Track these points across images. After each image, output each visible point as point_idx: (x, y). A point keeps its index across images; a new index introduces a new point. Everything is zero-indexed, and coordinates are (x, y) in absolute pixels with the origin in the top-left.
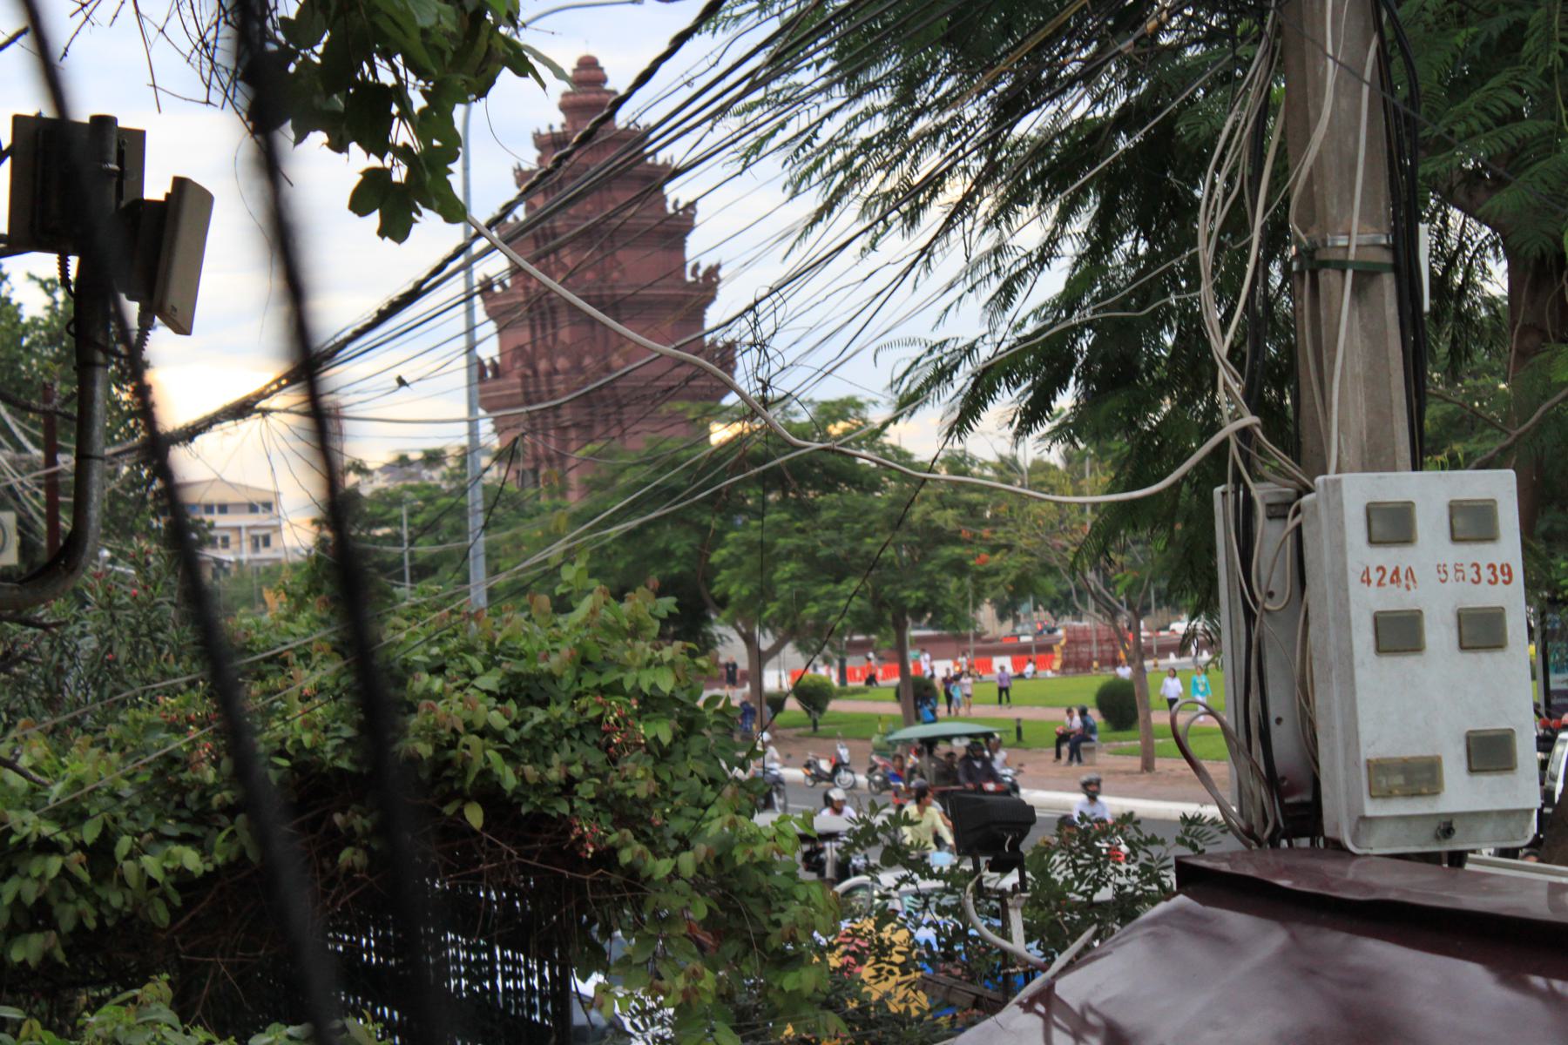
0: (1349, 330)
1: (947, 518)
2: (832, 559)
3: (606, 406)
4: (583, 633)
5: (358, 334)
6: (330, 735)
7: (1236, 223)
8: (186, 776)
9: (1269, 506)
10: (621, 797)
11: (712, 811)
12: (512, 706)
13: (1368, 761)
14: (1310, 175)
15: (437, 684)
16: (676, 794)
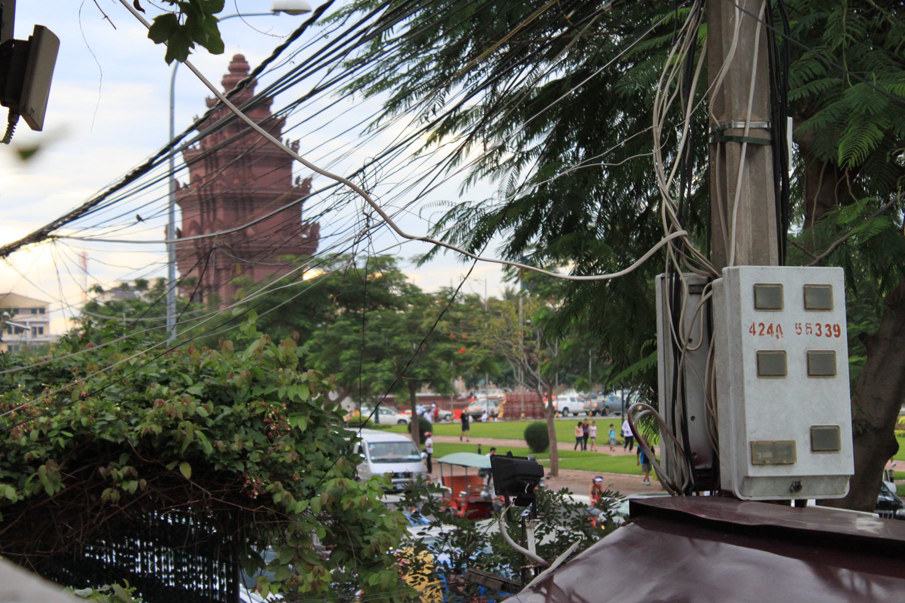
0: (743, 180)
1: (443, 326)
2: (374, 348)
3: (244, 253)
4: (254, 363)
5: (113, 190)
6: (98, 419)
7: (675, 110)
8: (8, 441)
9: (690, 286)
10: (275, 462)
11: (330, 473)
12: (211, 405)
13: (751, 443)
14: (722, 85)
15: (165, 390)
16: (308, 462)
